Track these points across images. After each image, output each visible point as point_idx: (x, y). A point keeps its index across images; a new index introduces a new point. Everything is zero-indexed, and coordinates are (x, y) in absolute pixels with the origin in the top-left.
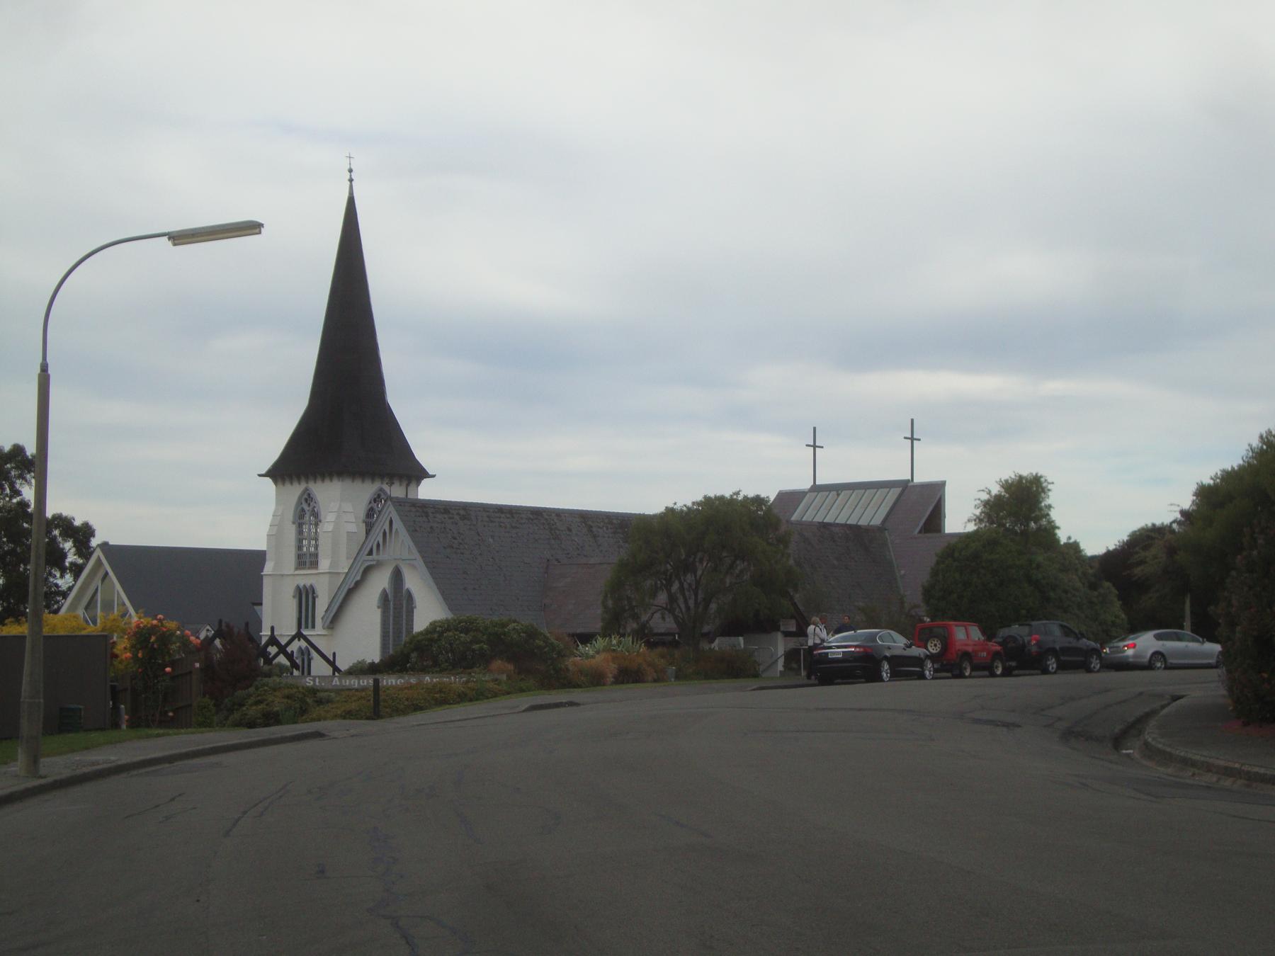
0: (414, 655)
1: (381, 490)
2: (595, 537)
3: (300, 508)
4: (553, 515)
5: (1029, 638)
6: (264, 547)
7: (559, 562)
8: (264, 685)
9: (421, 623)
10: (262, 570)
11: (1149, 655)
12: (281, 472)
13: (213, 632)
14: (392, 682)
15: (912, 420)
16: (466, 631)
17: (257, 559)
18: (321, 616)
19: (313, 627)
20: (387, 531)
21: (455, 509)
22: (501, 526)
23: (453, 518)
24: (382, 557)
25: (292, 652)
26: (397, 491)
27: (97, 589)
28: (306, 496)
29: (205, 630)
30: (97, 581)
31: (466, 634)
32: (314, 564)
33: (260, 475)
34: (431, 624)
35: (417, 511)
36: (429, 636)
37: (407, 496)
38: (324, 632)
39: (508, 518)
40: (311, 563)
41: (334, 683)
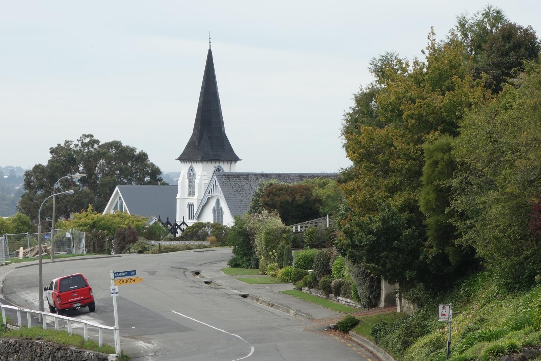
10: (176, 197)
23: (240, 179)
30: (117, 199)
32: (194, 195)
33: (176, 159)
35: (226, 177)
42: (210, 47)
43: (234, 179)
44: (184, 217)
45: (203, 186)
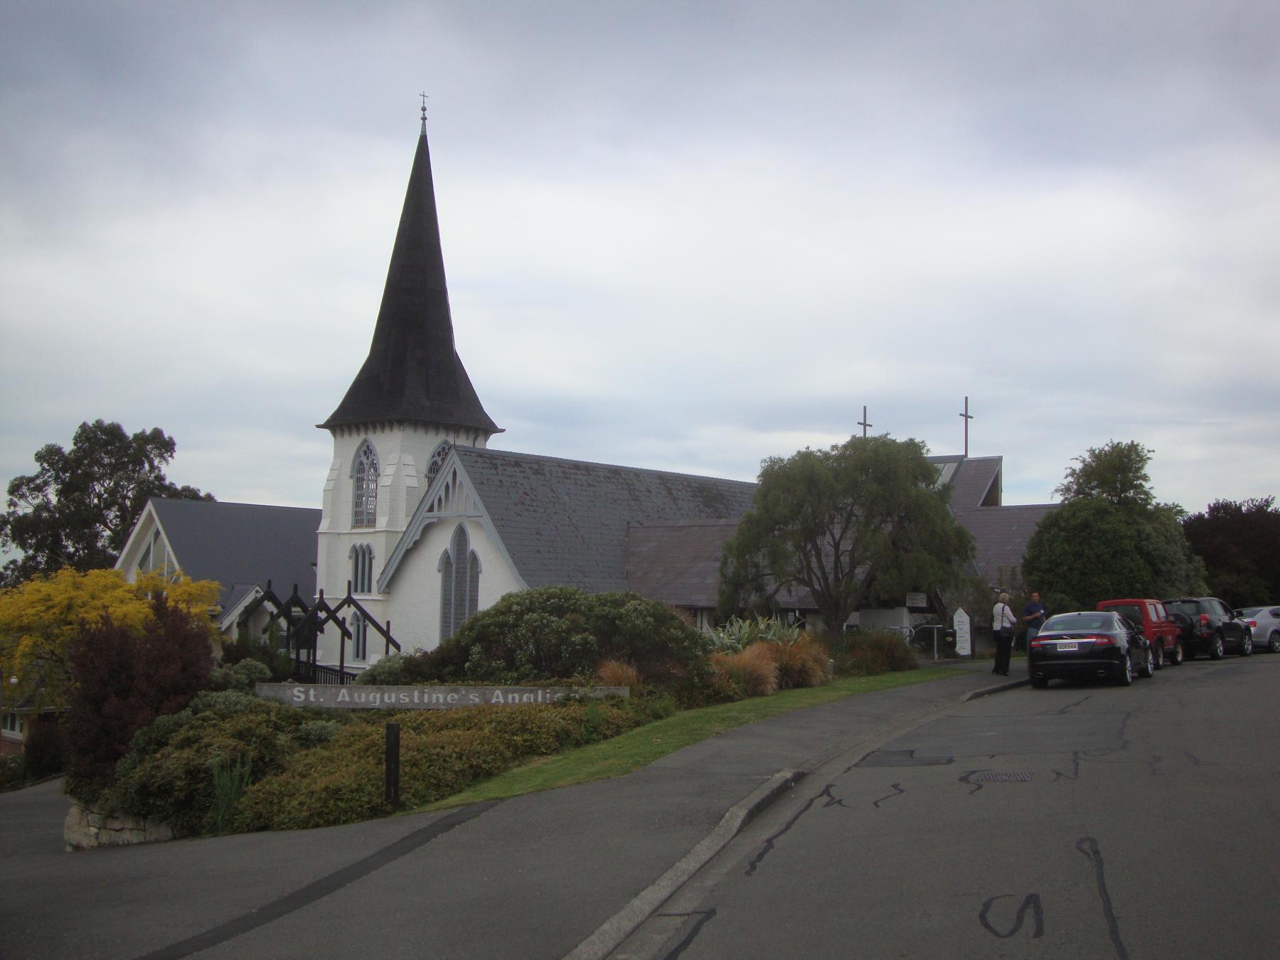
0: (476, 649)
1: (446, 442)
2: (674, 499)
3: (358, 461)
4: (632, 474)
5: (1198, 617)
6: (320, 507)
7: (642, 524)
8: (209, 706)
9: (489, 596)
11: (1269, 634)
12: (340, 423)
13: (262, 594)
14: (438, 699)
15: (966, 398)
16: (559, 611)
17: (315, 516)
18: (376, 581)
19: (370, 591)
20: (450, 484)
21: (527, 463)
22: (577, 483)
23: (525, 472)
24: (444, 513)
25: (344, 619)
26: (463, 441)
27: (149, 548)
28: (365, 448)
29: (254, 592)
30: (150, 538)
31: (560, 617)
32: (372, 522)
33: (318, 426)
34: (503, 599)
36: (501, 618)
37: (474, 446)
38: (379, 597)
39: (584, 475)
40: (369, 521)
41: (340, 699)
43: (508, 468)
45: (403, 494)
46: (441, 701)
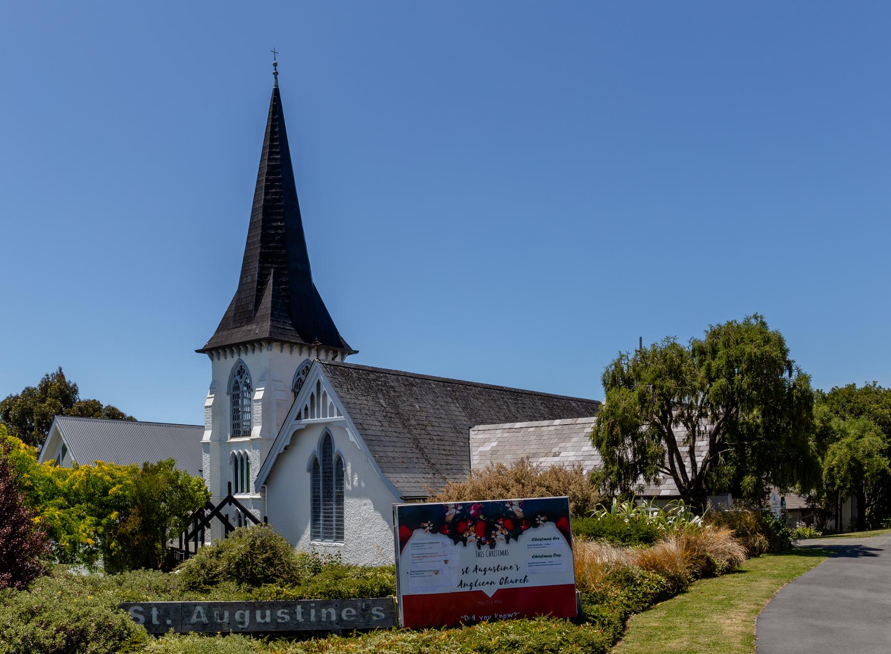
14: (329, 615)
19: (248, 491)
20: (315, 394)
33: (197, 351)
42: (276, 85)
44: (641, 338)
46: (334, 618)
